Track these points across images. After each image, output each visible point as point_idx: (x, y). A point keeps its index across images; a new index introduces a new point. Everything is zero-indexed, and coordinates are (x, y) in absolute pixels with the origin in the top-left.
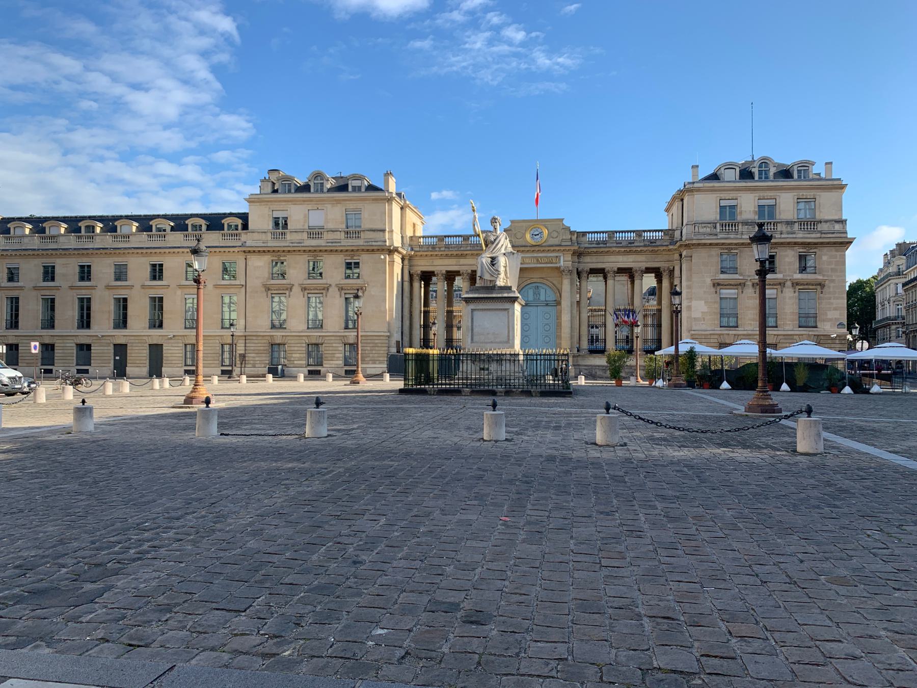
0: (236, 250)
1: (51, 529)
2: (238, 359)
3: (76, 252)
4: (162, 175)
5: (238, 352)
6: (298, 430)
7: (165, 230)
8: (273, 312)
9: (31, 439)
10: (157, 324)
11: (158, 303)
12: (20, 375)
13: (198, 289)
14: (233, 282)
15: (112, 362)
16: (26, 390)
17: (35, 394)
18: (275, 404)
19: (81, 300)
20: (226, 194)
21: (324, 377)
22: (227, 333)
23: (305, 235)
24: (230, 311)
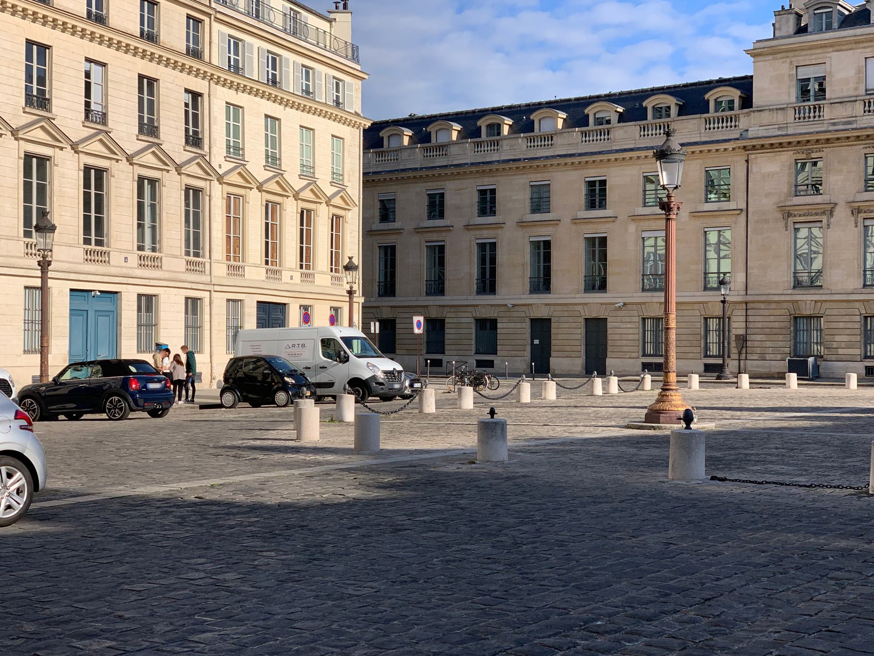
0: (729, 146)
1: (457, 613)
2: (733, 344)
3: (474, 169)
4: (607, 26)
5: (734, 332)
6: (853, 480)
7: (608, 122)
8: (797, 257)
9: (421, 469)
10: (598, 284)
11: (598, 248)
12: (399, 368)
13: (668, 220)
14: (725, 205)
15: (528, 348)
16: (408, 392)
17: (421, 400)
18: (805, 429)
19: (482, 247)
20: (714, 45)
21: (840, 381)
22: (714, 298)
23: (859, 108)
24: (719, 258)
